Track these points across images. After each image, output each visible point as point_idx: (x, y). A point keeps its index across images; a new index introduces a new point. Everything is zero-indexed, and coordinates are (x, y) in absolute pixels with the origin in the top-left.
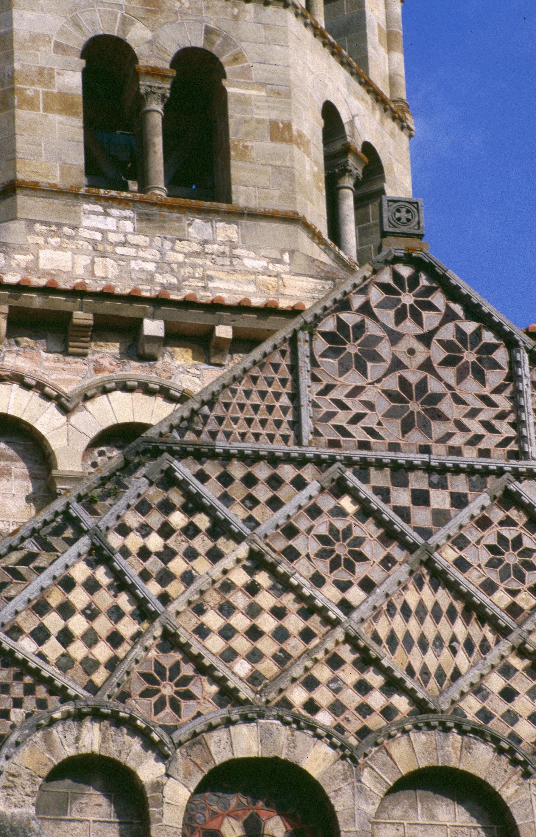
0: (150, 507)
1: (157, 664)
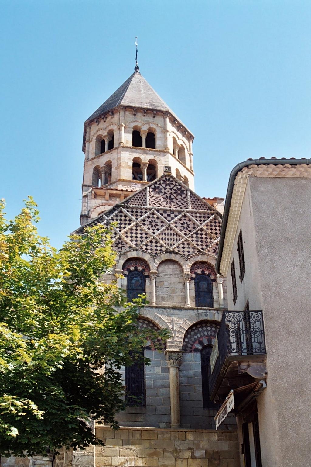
0: (118, 216)
1: (118, 241)
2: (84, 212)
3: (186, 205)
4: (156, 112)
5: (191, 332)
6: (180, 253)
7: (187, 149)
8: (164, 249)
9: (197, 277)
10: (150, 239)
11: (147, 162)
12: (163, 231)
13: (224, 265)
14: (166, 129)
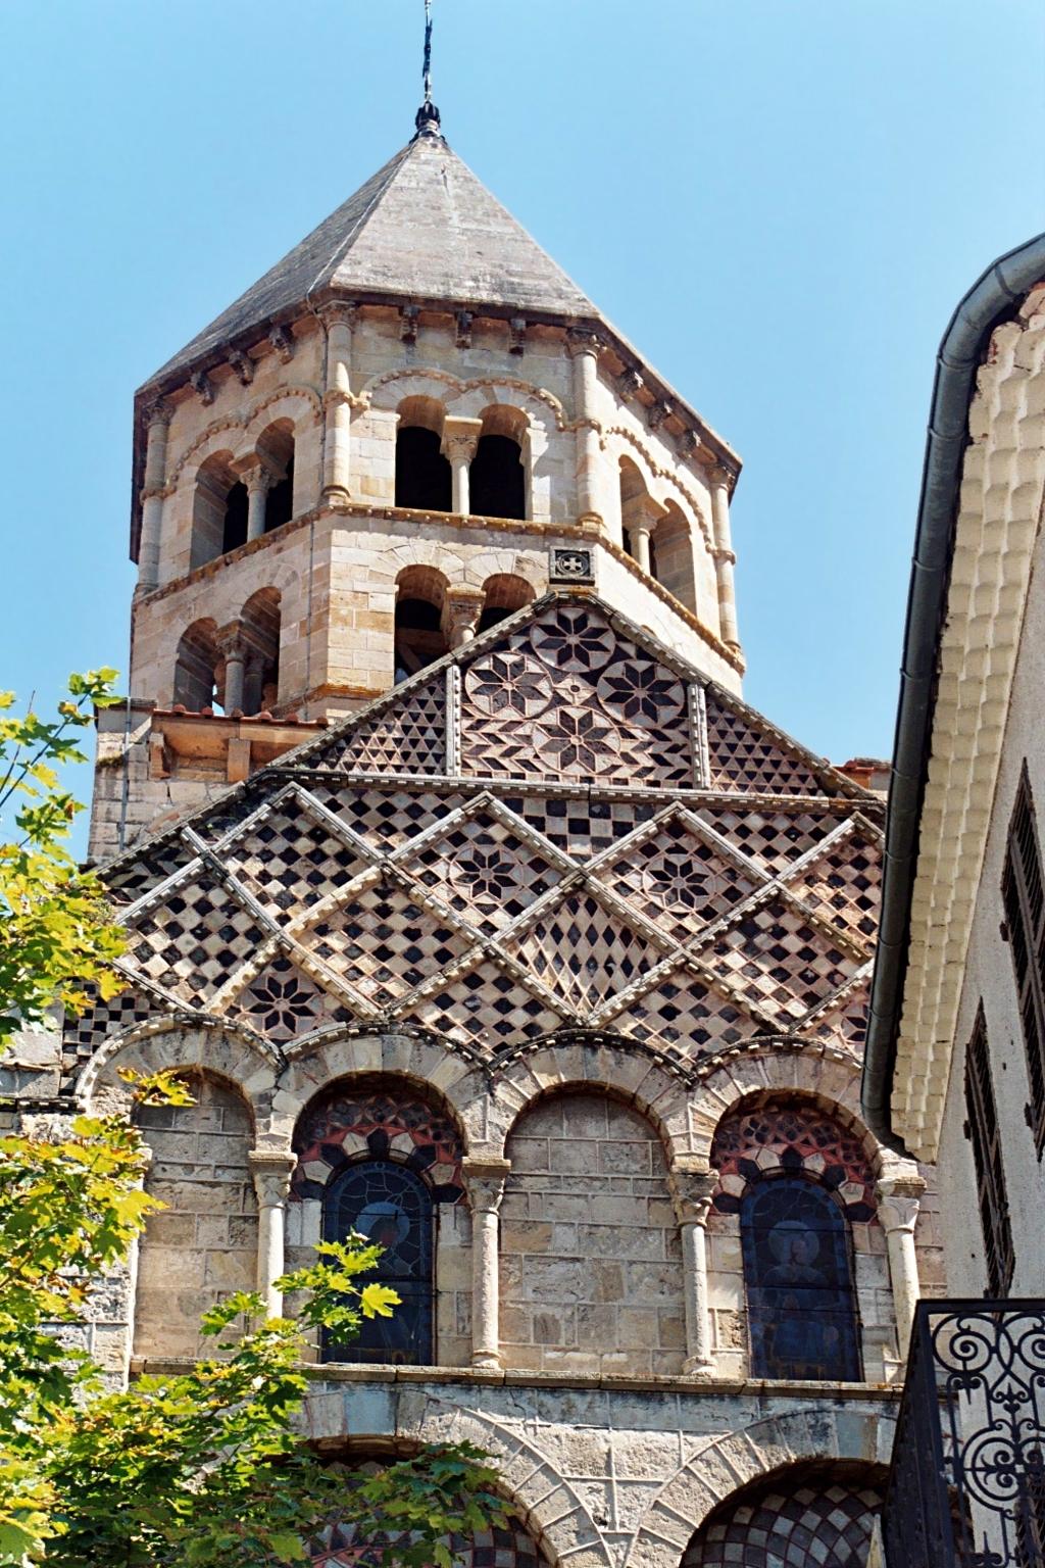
0: (274, 834)
1: (271, 980)
2: (102, 848)
3: (685, 765)
4: (528, 324)
5: (723, 1542)
6: (648, 1041)
7: (702, 526)
8: (547, 1021)
9: (753, 1194)
10: (466, 963)
11: (478, 591)
12: (543, 916)
13: (920, 1078)
14: (583, 413)
